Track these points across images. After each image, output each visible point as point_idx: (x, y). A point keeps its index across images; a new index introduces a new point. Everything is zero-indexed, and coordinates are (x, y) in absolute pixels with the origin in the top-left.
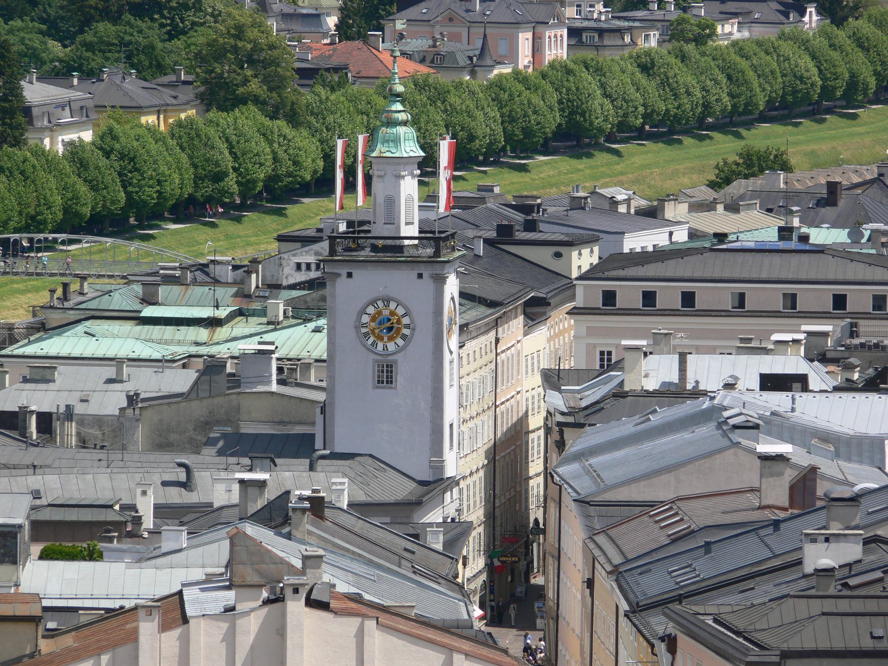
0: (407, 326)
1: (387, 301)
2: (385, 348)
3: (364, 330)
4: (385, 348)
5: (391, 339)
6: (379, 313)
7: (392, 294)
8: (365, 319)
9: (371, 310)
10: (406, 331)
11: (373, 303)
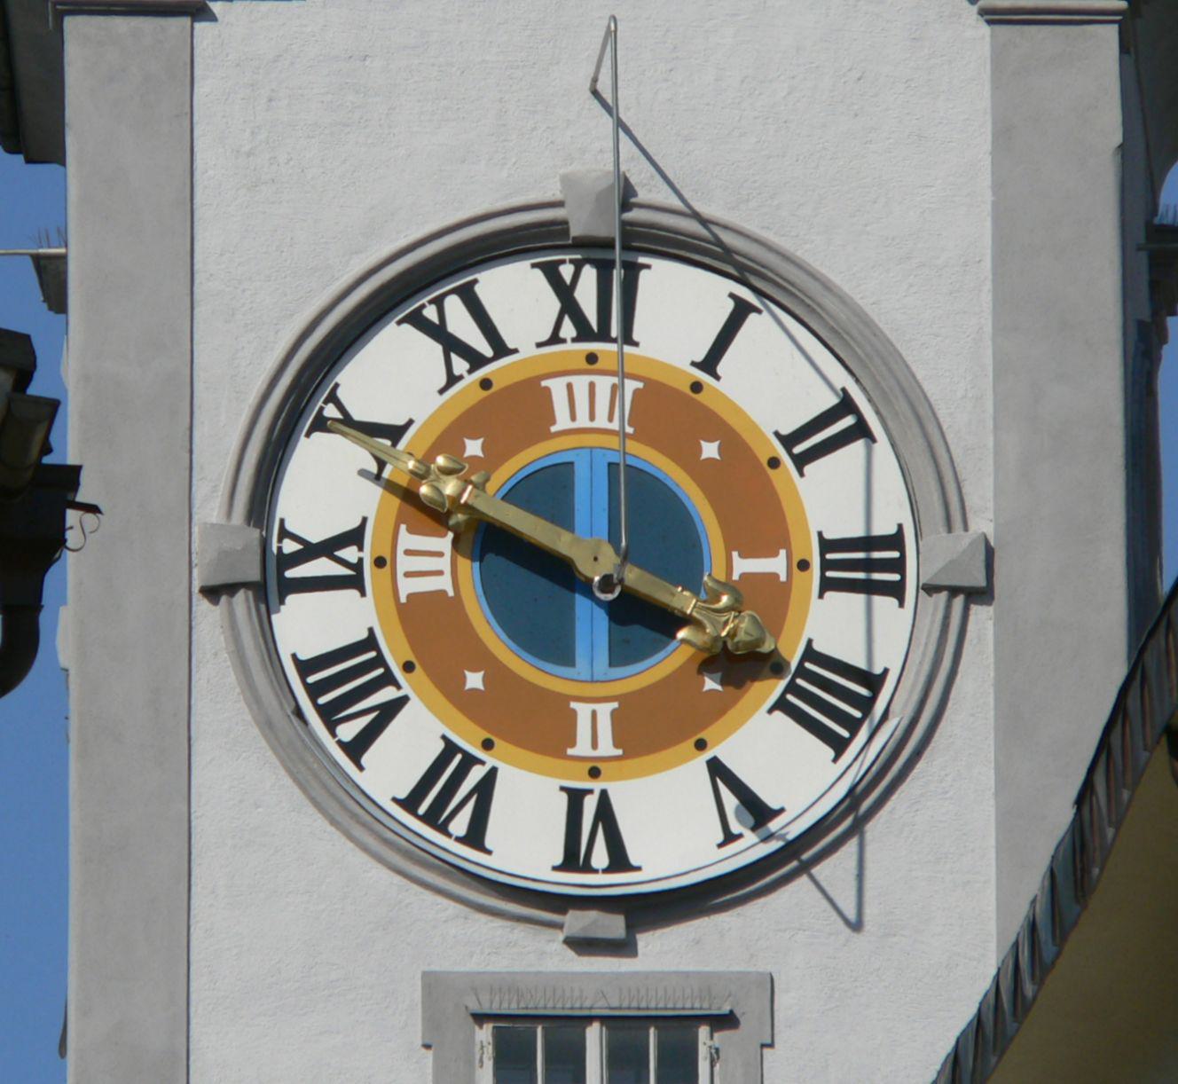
0: (865, 565)
2: (591, 827)
3: (312, 624)
4: (591, 827)
5: (648, 732)
6: (520, 410)
8: (326, 487)
9: (775, 380)
11: (415, 286)
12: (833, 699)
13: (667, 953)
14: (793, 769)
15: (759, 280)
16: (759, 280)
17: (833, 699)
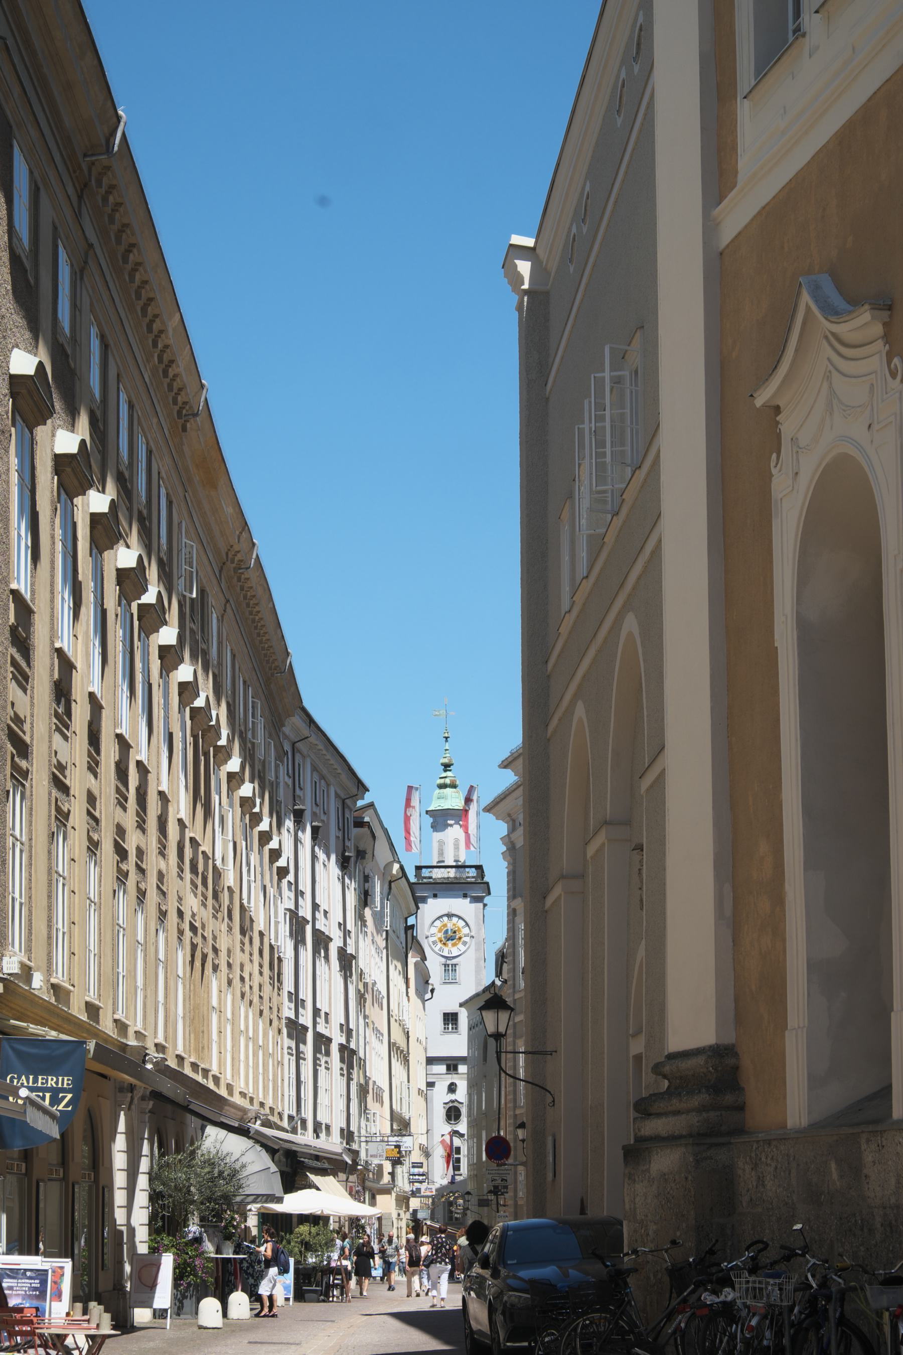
1: (450, 916)
3: (431, 939)
6: (445, 925)
7: (454, 912)
10: (467, 939)
12: (465, 943)
13: (454, 961)
14: (460, 946)
15: (460, 917)
16: (460, 917)
17: (465, 943)
